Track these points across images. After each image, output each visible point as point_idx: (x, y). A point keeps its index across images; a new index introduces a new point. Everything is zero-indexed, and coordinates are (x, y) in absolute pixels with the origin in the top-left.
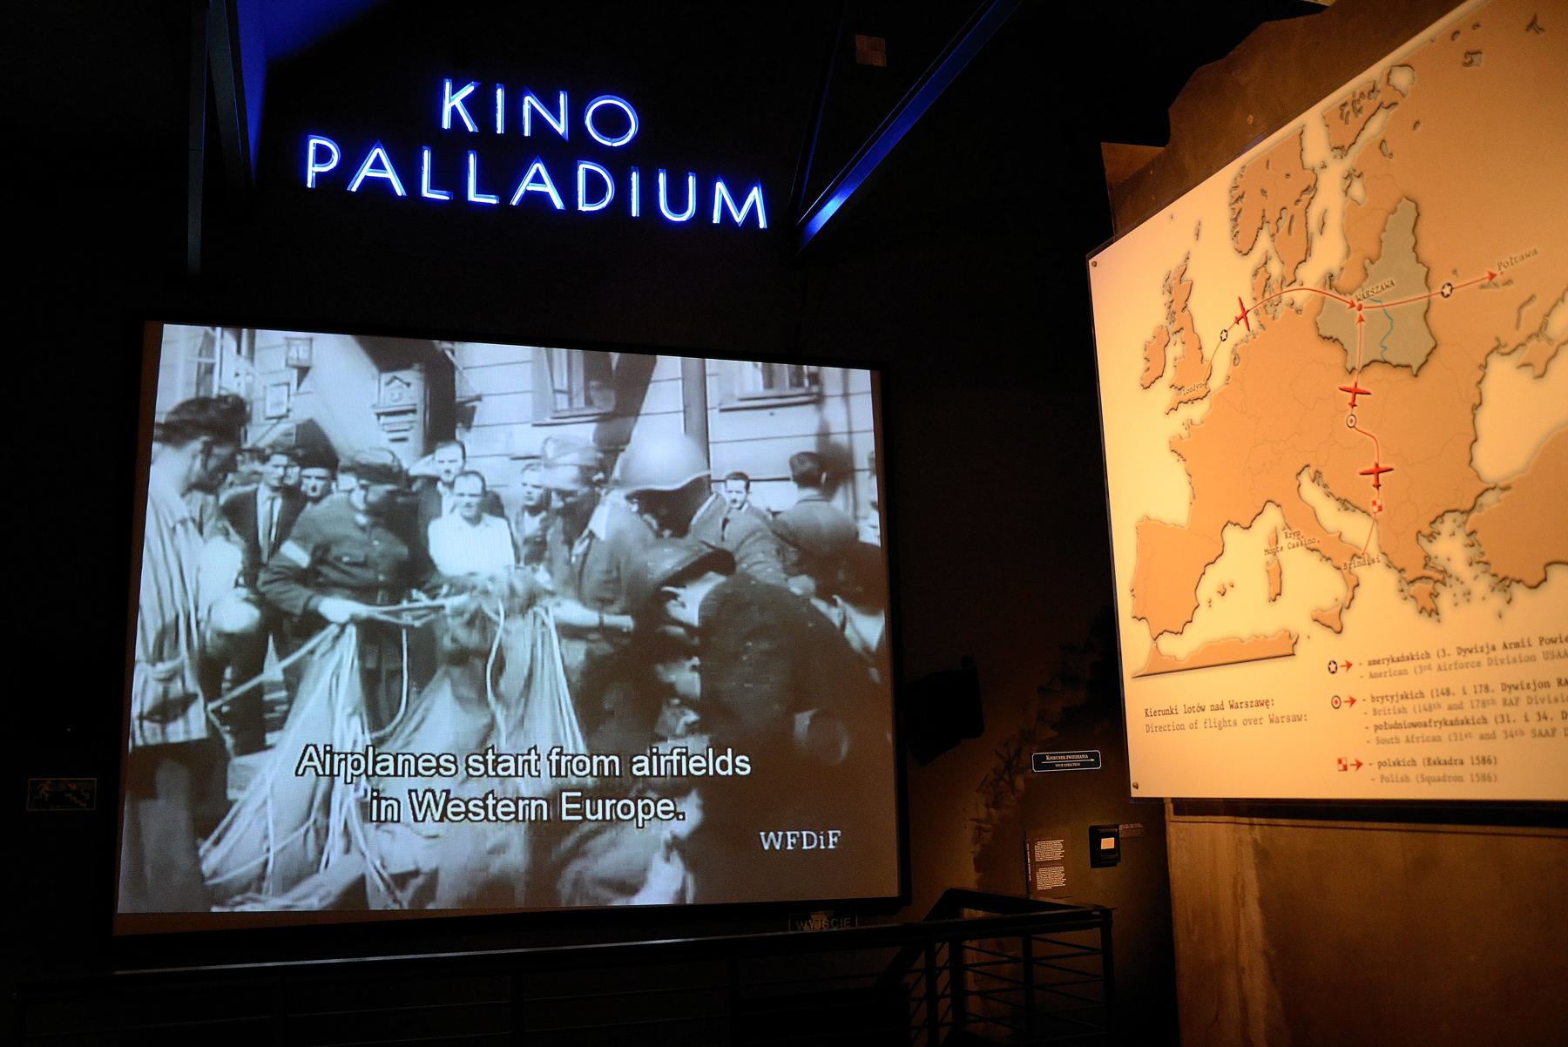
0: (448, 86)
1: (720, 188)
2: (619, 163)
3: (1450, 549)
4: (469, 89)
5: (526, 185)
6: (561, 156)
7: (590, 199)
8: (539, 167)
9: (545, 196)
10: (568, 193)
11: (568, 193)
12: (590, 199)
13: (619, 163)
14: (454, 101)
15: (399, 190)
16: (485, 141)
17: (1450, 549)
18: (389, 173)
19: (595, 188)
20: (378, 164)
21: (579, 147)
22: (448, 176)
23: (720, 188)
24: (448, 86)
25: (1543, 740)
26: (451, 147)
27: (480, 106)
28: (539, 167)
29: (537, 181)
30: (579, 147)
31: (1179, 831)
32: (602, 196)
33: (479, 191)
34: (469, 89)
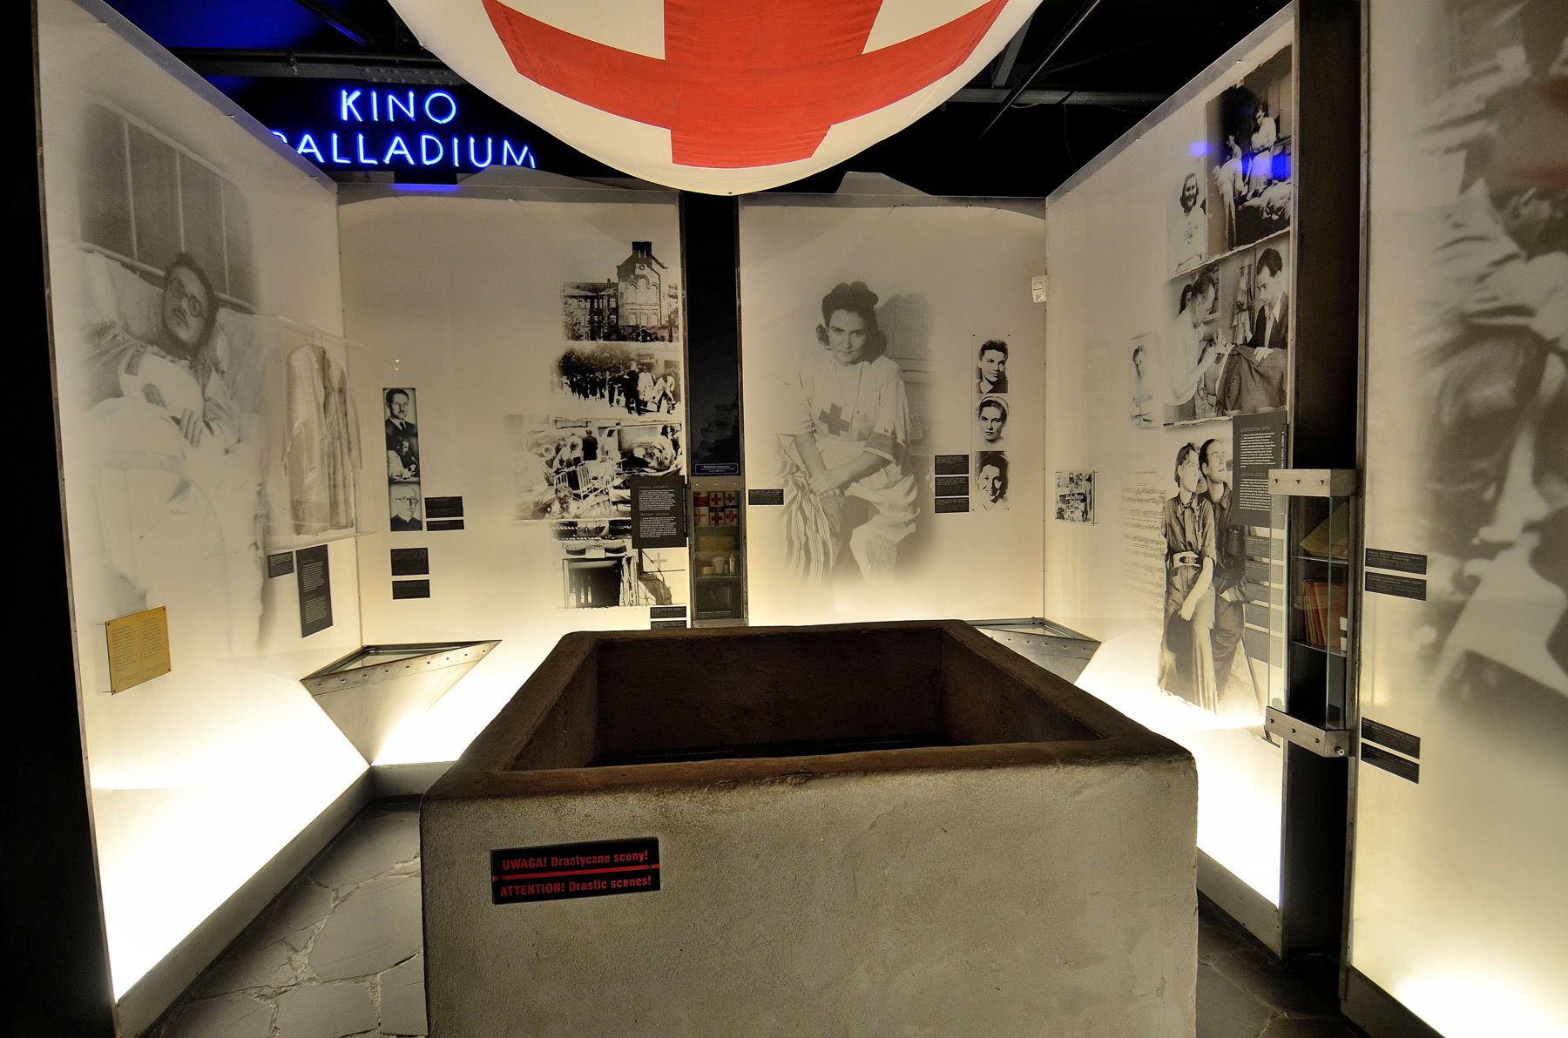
0: (344, 93)
1: (506, 144)
2: (445, 133)
3: (1275, 217)
4: (357, 94)
5: (392, 151)
6: (410, 130)
7: (428, 158)
8: (398, 139)
9: (403, 156)
10: (416, 153)
11: (416, 153)
12: (428, 158)
13: (445, 133)
14: (348, 101)
15: (411, 162)
16: (367, 127)
17: (1275, 217)
18: (405, 152)
19: (432, 153)
20: (308, 145)
21: (422, 124)
22: (348, 149)
23: (506, 144)
24: (344, 93)
25: (426, 444)
26: (348, 131)
27: (362, 104)
28: (398, 139)
29: (397, 147)
30: (422, 124)
31: (307, 589)
32: (437, 155)
33: (339, 156)
34: (357, 94)
